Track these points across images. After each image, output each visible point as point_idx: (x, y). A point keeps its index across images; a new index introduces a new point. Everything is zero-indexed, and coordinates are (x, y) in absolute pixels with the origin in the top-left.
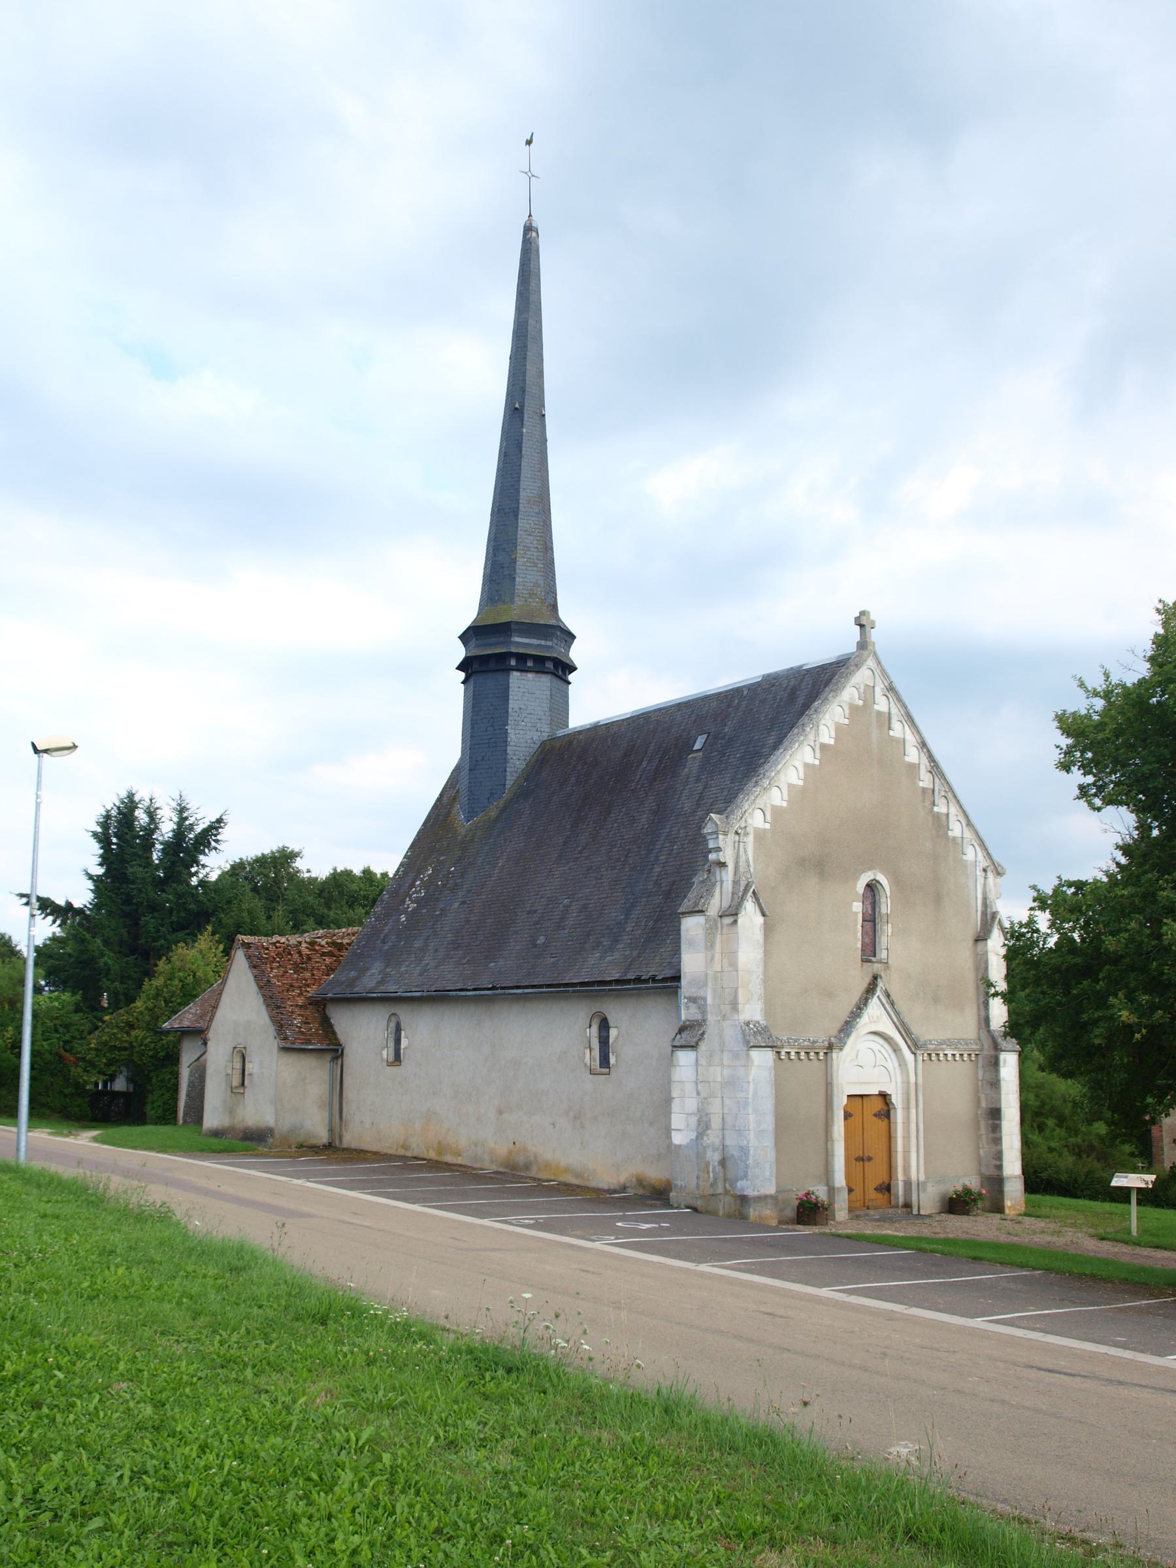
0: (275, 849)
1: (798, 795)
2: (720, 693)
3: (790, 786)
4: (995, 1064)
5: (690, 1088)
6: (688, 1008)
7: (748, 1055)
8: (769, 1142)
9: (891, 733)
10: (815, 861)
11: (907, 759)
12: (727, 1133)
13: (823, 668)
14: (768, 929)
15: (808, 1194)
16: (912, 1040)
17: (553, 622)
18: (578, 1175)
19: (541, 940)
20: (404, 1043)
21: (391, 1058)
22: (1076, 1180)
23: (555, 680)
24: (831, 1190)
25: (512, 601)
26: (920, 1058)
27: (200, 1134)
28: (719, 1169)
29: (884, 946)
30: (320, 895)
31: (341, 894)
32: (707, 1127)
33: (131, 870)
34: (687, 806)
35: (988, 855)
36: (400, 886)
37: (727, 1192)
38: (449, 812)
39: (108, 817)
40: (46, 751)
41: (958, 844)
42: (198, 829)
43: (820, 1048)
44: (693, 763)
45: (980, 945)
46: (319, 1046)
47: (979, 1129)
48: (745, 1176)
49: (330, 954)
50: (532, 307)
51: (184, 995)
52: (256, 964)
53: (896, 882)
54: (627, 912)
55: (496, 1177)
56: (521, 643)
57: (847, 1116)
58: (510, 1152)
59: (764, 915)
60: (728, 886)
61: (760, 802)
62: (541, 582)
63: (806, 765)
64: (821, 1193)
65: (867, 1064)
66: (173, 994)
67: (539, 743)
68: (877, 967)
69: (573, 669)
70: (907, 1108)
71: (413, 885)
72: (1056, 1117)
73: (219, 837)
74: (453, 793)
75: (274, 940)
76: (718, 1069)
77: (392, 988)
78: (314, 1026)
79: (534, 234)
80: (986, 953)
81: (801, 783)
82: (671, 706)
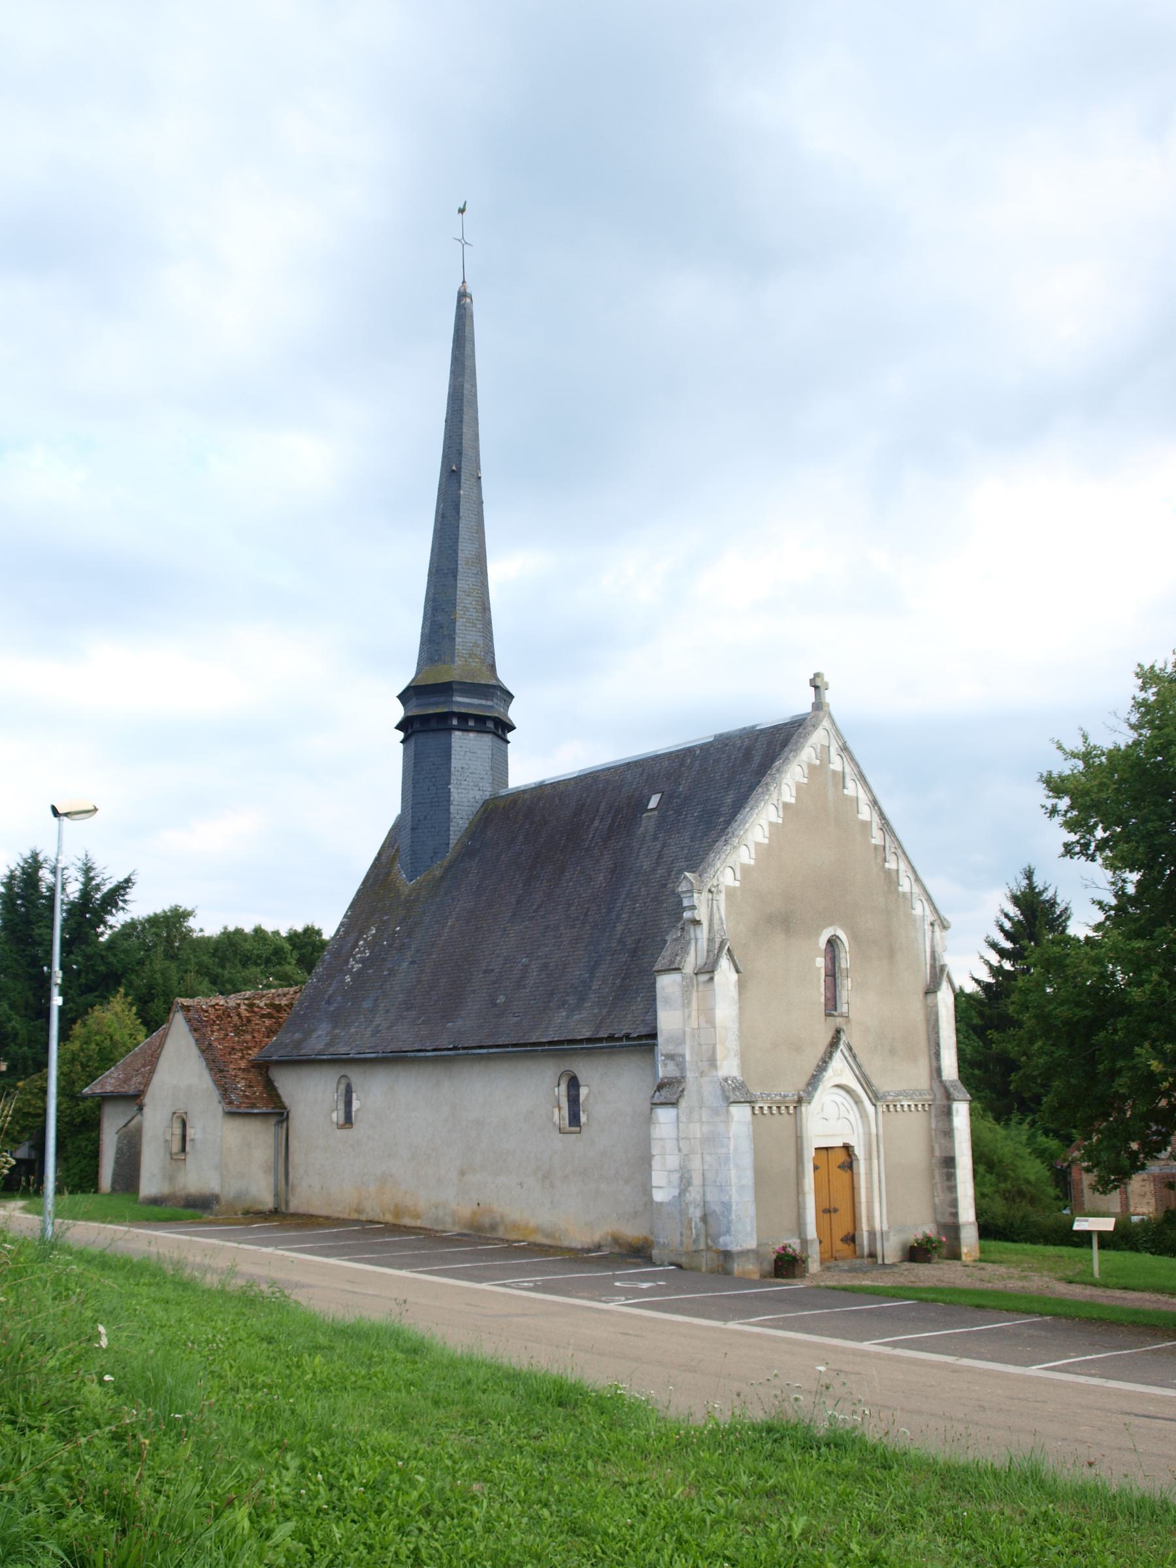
0: (167, 908)
1: (765, 853)
2: (671, 753)
3: (757, 844)
4: (948, 1113)
5: (671, 1145)
6: (666, 1065)
7: (728, 1111)
8: (749, 1197)
9: (846, 792)
10: (782, 919)
11: (860, 817)
12: (708, 1189)
13: (777, 729)
14: (742, 985)
15: (784, 1248)
16: (873, 1092)
17: (493, 682)
18: (547, 1235)
19: (501, 999)
20: (356, 1105)
21: (342, 1121)
22: (1012, 1225)
23: (496, 739)
24: (804, 1242)
25: (453, 662)
26: (880, 1110)
27: (136, 1201)
28: (701, 1225)
29: (844, 1000)
30: (214, 955)
31: (235, 953)
32: (689, 1184)
33: (37, 931)
34: (646, 866)
35: (935, 910)
36: (341, 947)
37: (708, 1248)
38: (390, 872)
39: (12, 877)
40: (66, 815)
41: (907, 899)
42: (105, 889)
43: (791, 1102)
44: (648, 823)
45: (930, 997)
46: (264, 1110)
47: (933, 1177)
48: (728, 1232)
49: (269, 1016)
50: (468, 371)
51: (102, 1060)
52: (197, 1027)
53: (854, 937)
54: (592, 970)
55: (459, 1239)
56: (462, 702)
57: (816, 1168)
58: (474, 1213)
59: (738, 971)
60: (703, 944)
61: (730, 861)
62: (481, 642)
63: (771, 824)
64: (794, 1244)
65: (831, 1118)
66: (90, 1058)
67: (481, 802)
68: (839, 1021)
69: (511, 728)
70: (869, 1159)
71: (356, 945)
72: (985, 1163)
73: (127, 897)
74: (392, 852)
75: (213, 1003)
76: (698, 1125)
77: (343, 1049)
78: (258, 1090)
79: (468, 300)
80: (936, 1006)
81: (766, 841)
82: (620, 766)
